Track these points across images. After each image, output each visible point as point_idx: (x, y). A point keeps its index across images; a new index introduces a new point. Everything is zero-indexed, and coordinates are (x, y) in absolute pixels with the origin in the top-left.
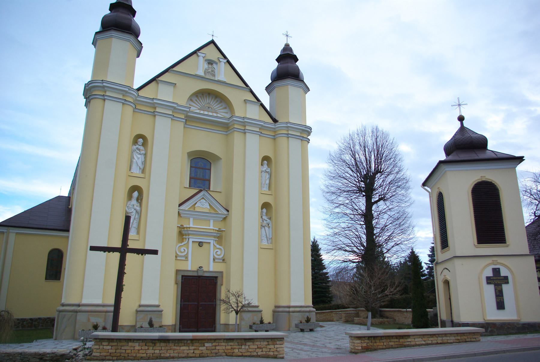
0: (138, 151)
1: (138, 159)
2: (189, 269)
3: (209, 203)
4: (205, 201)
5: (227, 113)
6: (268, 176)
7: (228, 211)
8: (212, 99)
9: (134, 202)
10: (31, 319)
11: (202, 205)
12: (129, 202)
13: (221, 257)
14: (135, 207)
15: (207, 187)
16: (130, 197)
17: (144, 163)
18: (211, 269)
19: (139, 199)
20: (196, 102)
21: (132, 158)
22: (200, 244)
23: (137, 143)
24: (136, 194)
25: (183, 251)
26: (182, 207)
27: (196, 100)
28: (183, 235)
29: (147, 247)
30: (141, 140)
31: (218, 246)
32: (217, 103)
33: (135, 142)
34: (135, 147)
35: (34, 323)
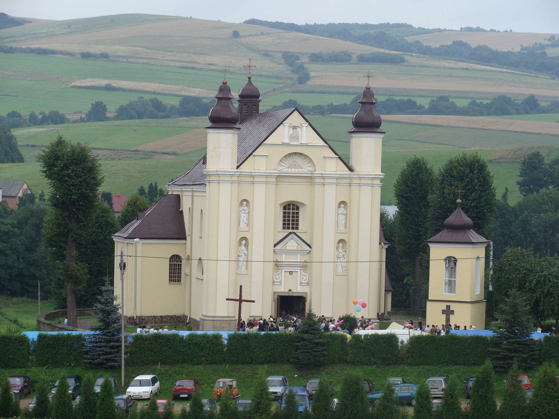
0: (243, 212)
1: (244, 217)
2: (283, 291)
3: (297, 242)
4: (293, 241)
5: (310, 167)
6: (344, 217)
7: (310, 247)
8: (298, 157)
9: (243, 248)
10: (161, 316)
11: (292, 244)
12: (240, 248)
13: (306, 282)
14: (244, 252)
15: (296, 226)
16: (240, 244)
17: (248, 219)
18: (299, 291)
19: (246, 245)
20: (285, 162)
21: (239, 217)
22: (291, 273)
23: (242, 204)
24: (244, 242)
25: (278, 278)
26: (277, 248)
27: (285, 160)
28: (278, 267)
29: (252, 300)
30: (245, 203)
31: (304, 274)
32: (303, 159)
33: (241, 204)
34: (241, 209)
35: (163, 319)
